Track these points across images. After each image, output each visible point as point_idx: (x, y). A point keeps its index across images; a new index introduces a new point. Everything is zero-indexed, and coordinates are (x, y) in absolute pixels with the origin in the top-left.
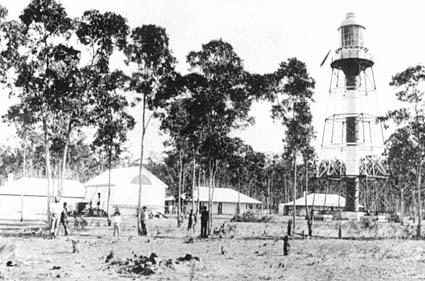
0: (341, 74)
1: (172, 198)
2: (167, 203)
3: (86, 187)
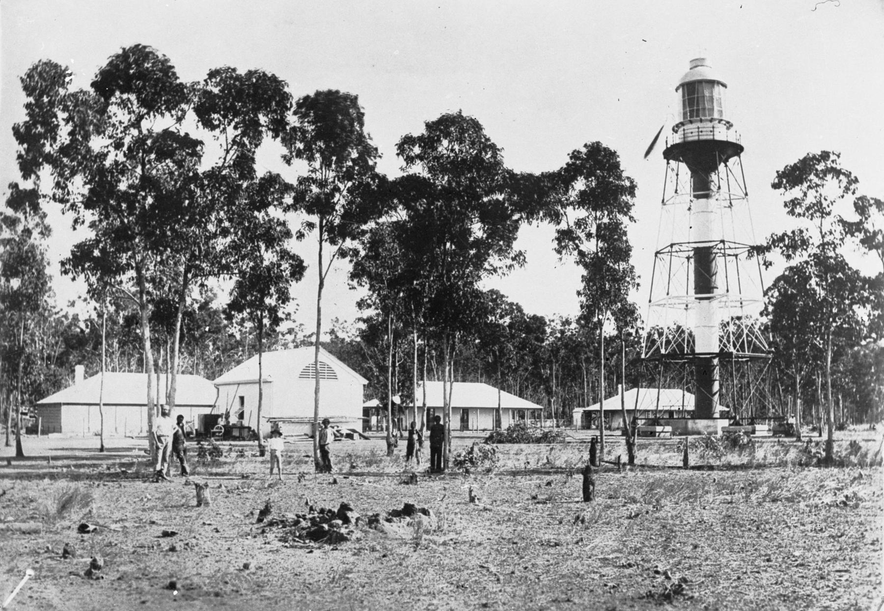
0: (684, 170)
1: (374, 403)
2: (367, 412)
3: (217, 387)
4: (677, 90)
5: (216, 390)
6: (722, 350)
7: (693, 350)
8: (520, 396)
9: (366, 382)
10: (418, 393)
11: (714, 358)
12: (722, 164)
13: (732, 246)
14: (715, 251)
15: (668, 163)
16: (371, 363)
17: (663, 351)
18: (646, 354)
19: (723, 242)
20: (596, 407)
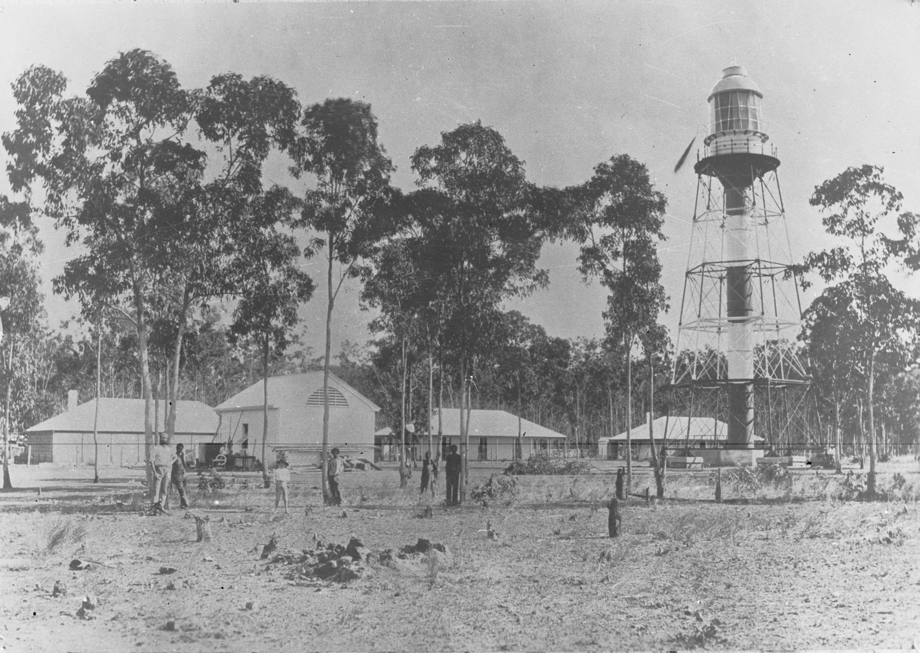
0: (716, 183)
2: (379, 441)
3: (220, 413)
4: (709, 100)
5: (217, 417)
6: (757, 376)
7: (726, 377)
8: (542, 425)
9: (378, 409)
10: (434, 421)
11: (749, 384)
12: (757, 179)
13: (768, 265)
14: (750, 271)
15: (700, 178)
16: (383, 389)
17: (694, 377)
18: (676, 380)
19: (758, 261)
20: (623, 436)
